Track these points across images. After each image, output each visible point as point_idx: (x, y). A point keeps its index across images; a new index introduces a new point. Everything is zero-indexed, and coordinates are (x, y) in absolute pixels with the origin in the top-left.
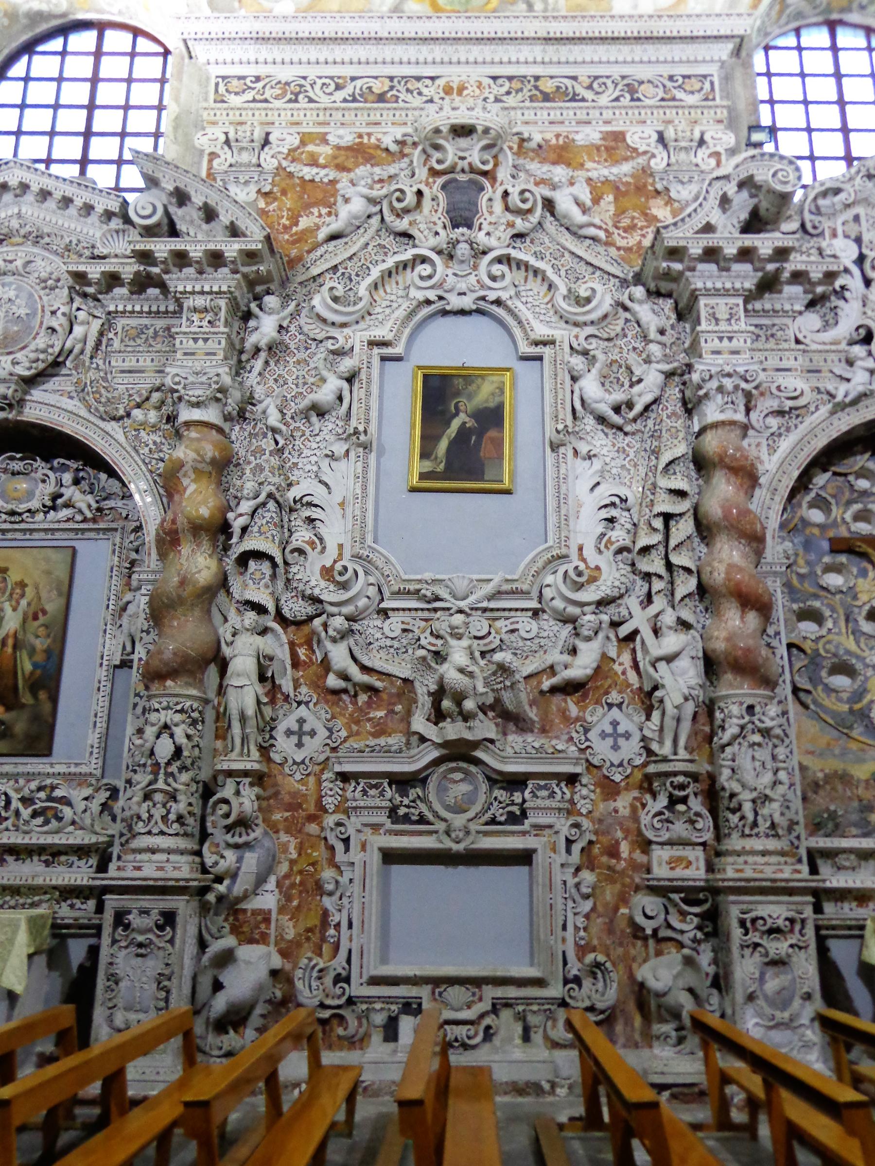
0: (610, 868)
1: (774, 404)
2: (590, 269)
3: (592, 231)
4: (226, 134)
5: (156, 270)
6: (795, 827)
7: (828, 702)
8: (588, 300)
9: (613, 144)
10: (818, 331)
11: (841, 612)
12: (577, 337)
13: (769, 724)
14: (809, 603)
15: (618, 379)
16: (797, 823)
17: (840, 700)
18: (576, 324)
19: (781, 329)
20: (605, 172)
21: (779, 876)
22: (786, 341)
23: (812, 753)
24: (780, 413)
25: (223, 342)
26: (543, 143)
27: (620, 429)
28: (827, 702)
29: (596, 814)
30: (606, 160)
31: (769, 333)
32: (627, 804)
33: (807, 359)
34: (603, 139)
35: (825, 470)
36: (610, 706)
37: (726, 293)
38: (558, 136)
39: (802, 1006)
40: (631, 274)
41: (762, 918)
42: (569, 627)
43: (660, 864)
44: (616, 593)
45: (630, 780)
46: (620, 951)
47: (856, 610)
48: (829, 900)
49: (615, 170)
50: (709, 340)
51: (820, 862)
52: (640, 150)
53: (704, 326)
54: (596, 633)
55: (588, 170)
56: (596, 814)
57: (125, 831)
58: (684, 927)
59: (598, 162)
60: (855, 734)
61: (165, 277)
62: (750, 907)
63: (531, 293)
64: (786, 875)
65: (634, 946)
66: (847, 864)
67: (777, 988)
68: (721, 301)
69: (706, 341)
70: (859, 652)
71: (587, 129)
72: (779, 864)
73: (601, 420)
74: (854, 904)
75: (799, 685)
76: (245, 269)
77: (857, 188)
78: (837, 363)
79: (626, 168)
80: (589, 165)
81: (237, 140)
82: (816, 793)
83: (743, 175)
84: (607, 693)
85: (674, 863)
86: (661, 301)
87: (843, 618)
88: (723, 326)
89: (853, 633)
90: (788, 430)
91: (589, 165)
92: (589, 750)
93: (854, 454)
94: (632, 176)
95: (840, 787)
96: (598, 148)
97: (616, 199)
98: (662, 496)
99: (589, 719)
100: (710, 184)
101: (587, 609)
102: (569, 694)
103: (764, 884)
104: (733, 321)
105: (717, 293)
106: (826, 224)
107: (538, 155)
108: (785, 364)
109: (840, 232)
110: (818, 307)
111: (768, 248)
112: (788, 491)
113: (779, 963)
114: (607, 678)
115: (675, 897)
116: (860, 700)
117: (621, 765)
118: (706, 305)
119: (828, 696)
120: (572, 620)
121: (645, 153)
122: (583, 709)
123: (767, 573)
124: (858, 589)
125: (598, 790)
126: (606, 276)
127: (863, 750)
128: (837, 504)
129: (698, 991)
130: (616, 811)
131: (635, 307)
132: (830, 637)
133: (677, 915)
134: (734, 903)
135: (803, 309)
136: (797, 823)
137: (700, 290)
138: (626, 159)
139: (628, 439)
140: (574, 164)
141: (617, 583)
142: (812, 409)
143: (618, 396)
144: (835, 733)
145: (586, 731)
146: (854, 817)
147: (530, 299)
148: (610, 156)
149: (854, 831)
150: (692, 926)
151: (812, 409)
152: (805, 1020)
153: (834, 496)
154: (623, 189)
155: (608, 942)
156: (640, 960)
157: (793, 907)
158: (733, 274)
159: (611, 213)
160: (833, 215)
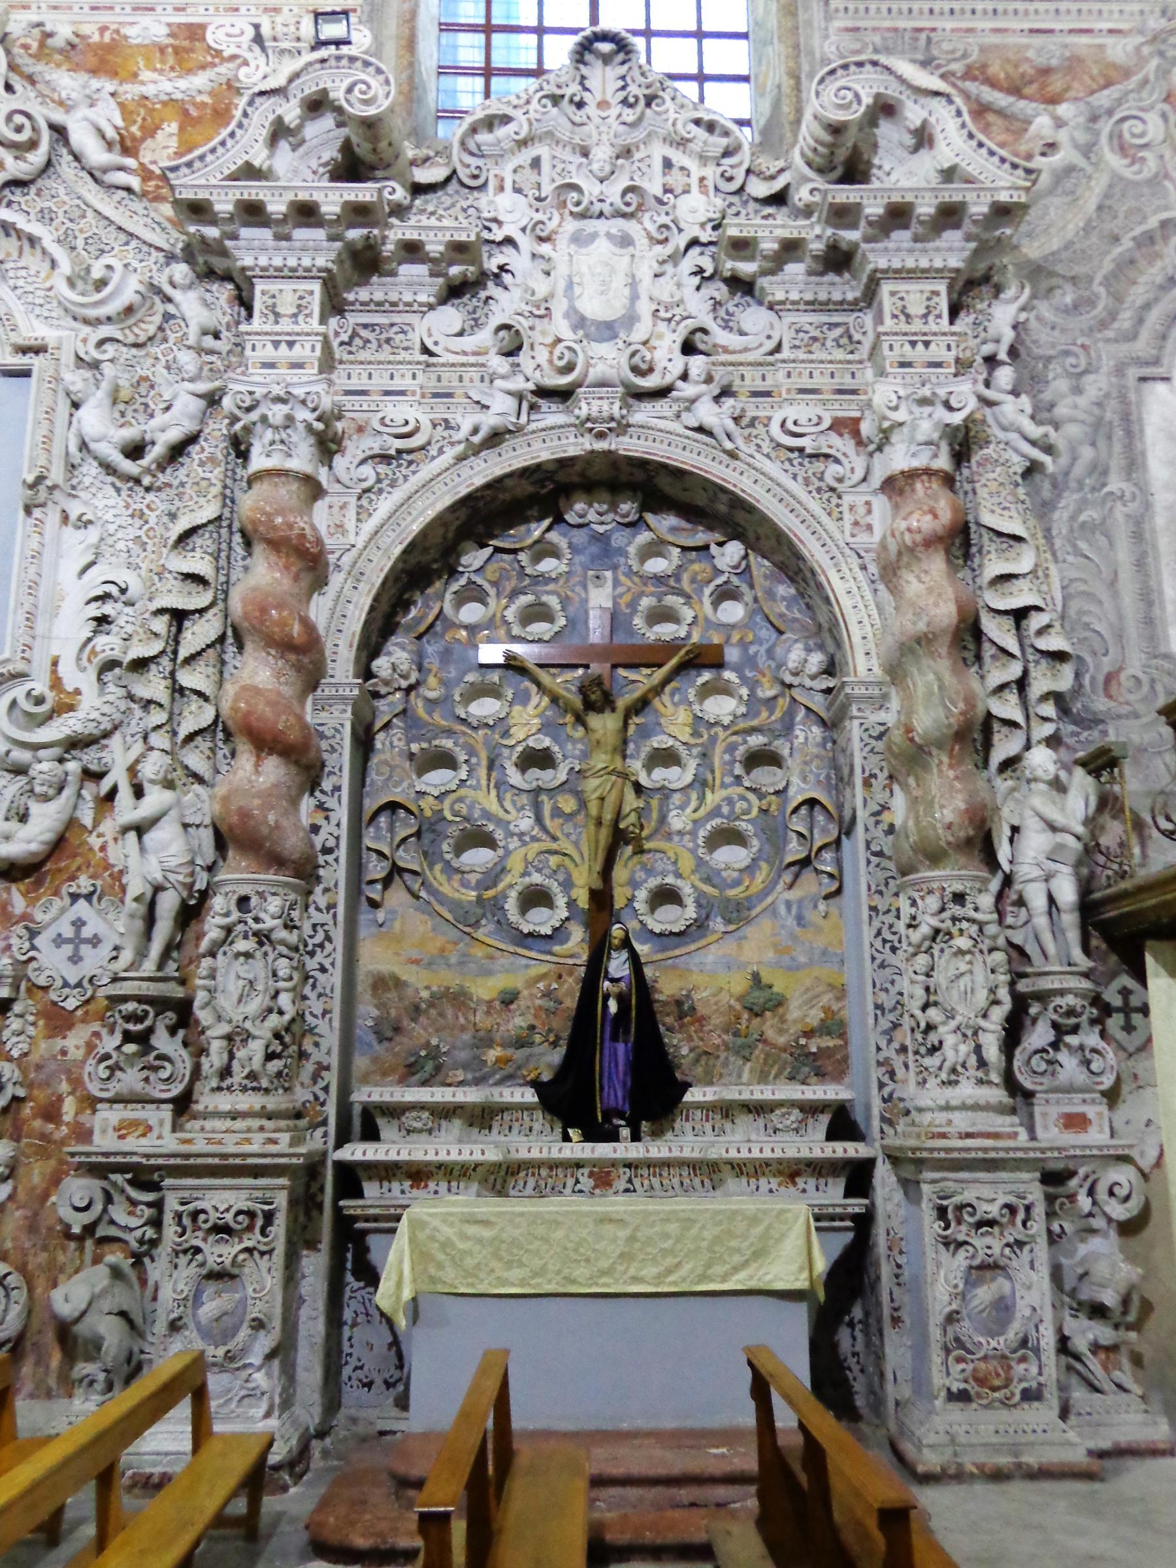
0: (43, 1136)
1: (373, 444)
2: (123, 237)
3: (121, 178)
4: (257, 27)
5: (212, 232)
6: (324, 1073)
7: (447, 888)
8: (101, 284)
9: (186, 43)
10: (461, 334)
11: (484, 755)
12: (85, 341)
13: (269, 923)
14: (436, 742)
15: (146, 405)
16: (327, 1068)
17: (465, 884)
18: (86, 321)
19: (403, 332)
20: (167, 86)
21: (247, 1148)
22: (406, 349)
23: (417, 962)
24: (385, 458)
25: (318, 347)
26: (76, 40)
27: (138, 481)
28: (446, 889)
29: (34, 1058)
30: (172, 69)
31: (384, 336)
32: (81, 1042)
33: (434, 377)
34: (172, 35)
35: (483, 545)
36: (75, 897)
37: (293, 274)
38: (103, 29)
39: (252, 1338)
40: (180, 245)
41: (203, 1211)
42: (22, 780)
43: (104, 1131)
44: (106, 725)
45: (91, 1007)
46: (43, 1257)
47: (506, 752)
48: (370, 1179)
49: (182, 84)
50: (259, 345)
51: (381, 1122)
52: (226, 54)
53: (889, 324)
54: (60, 790)
55: (143, 83)
56: (34, 1058)
57: (886, 1079)
58: (134, 1222)
59: (161, 72)
60: (480, 934)
61: (229, 243)
62: (196, 1194)
63: (23, 273)
64: (255, 1148)
65: (64, 1249)
66: (418, 1125)
67: (217, 1313)
68: (288, 286)
69: (254, 348)
70: (501, 813)
71: (145, 20)
72: (249, 1130)
73: (109, 468)
74: (407, 1184)
75: (401, 864)
76: (354, 234)
77: (532, 115)
78: (477, 383)
79: (200, 81)
80: (146, 75)
81: (275, 39)
82: (414, 1020)
83: (310, 89)
84: (73, 878)
85: (123, 1129)
86: (215, 287)
87: (484, 763)
88: (917, 326)
89: (497, 787)
90: (393, 484)
91: (146, 75)
92: (34, 964)
93: (526, 520)
94: (211, 93)
95: (450, 1012)
96: (162, 50)
97: (182, 129)
98: (172, 582)
99: (39, 916)
100: (251, 103)
101: (42, 753)
102: (14, 880)
103: (210, 1161)
104: (301, 318)
105: (280, 274)
106: (491, 172)
107: (68, 58)
108: (398, 384)
109: (508, 185)
110: (465, 299)
111: (333, 203)
112: (382, 575)
113: (220, 1276)
114: (75, 856)
115: (117, 1178)
116: (495, 885)
117: (79, 985)
118: (263, 293)
119: (449, 879)
120: (19, 770)
121: (234, 57)
122: (32, 902)
123: (331, 698)
124: (511, 722)
125: (41, 1023)
126: (145, 248)
127: (491, 957)
128: (498, 595)
129: (133, 1316)
130: (64, 1053)
131: (176, 295)
132: (463, 792)
133: (126, 1205)
134: (174, 1188)
135: (432, 300)
136: (327, 1068)
137: (252, 269)
138: (203, 67)
139: (150, 497)
140: (123, 74)
141: (95, 715)
142: (434, 452)
143: (130, 434)
144: (453, 933)
145: (33, 934)
146: (463, 1055)
147: (20, 283)
148: (180, 62)
149: (460, 1075)
150: (140, 1222)
151: (434, 452)
152: (255, 1359)
153: (494, 584)
154: (194, 112)
155: (27, 1245)
156: (70, 1270)
157: (259, 1194)
158: (298, 244)
159: (171, 151)
160: (499, 158)
